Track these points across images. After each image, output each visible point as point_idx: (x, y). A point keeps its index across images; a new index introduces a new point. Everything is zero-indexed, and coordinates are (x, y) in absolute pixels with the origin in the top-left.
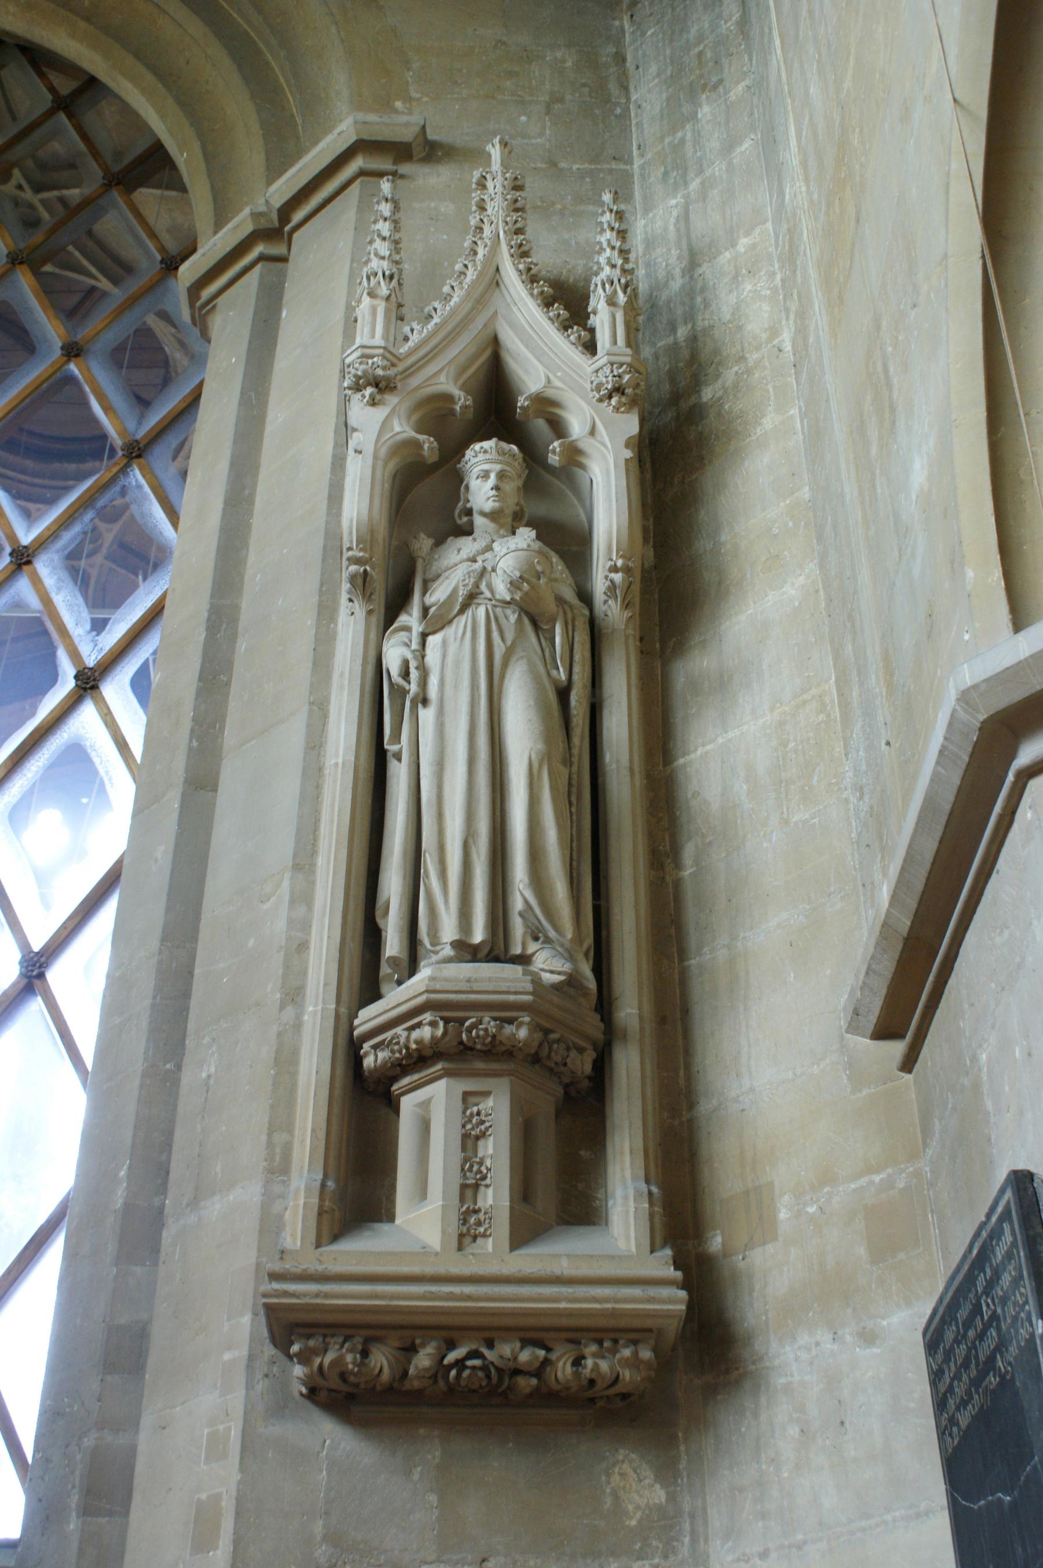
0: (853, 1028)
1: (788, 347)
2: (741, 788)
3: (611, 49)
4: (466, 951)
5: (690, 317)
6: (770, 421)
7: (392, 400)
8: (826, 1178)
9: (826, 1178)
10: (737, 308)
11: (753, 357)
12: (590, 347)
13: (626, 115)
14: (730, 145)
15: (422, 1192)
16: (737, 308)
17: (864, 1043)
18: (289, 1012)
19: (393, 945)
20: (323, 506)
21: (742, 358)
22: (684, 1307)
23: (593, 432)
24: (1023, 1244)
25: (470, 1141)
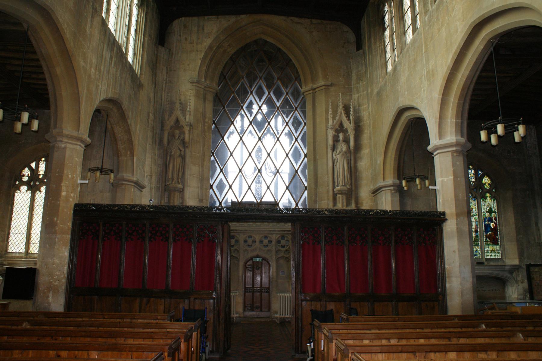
0: (370, 192)
1: (368, 123)
2: (362, 169)
3: (349, 66)
4: (342, 186)
5: (359, 113)
6: (366, 131)
7: (333, 129)
8: (367, 203)
9: (367, 203)
10: (363, 115)
11: (365, 122)
12: (350, 123)
13: (351, 78)
14: (363, 91)
15: (339, 203)
16: (363, 115)
17: (370, 194)
18: (328, 188)
19: (336, 184)
20: (325, 135)
21: (364, 122)
22: (191, 201)
23: (351, 133)
24: (465, 88)
25: (343, 200)
